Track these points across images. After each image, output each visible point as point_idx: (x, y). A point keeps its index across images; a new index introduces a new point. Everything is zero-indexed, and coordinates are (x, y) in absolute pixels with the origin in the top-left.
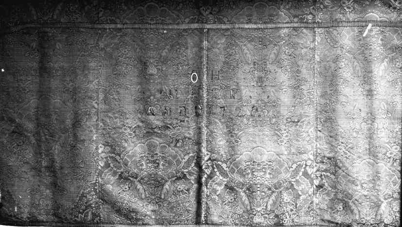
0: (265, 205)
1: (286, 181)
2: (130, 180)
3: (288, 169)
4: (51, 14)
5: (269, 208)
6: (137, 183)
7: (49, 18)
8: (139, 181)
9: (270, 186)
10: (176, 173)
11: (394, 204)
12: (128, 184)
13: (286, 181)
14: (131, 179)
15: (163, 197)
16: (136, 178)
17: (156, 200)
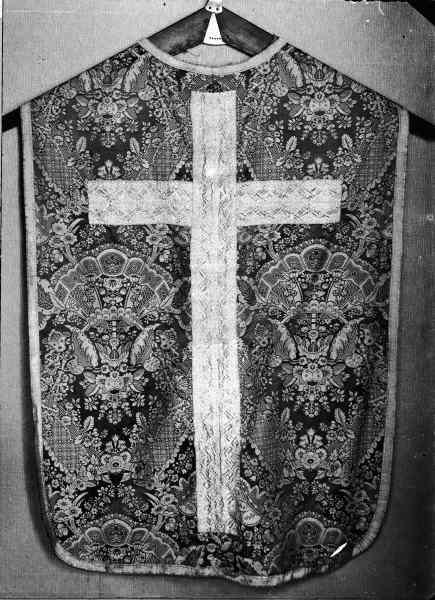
0: (326, 350)
1: (165, 313)
2: (68, 330)
3: (168, 288)
4: (120, 82)
5: (334, 356)
6: (83, 338)
7: (116, 89)
8: (87, 333)
9: (337, 315)
10: (364, 310)
11: (162, 337)
12: (64, 338)
13: (165, 313)
14: (72, 329)
15: (133, 362)
16: (81, 327)
17: (319, 362)
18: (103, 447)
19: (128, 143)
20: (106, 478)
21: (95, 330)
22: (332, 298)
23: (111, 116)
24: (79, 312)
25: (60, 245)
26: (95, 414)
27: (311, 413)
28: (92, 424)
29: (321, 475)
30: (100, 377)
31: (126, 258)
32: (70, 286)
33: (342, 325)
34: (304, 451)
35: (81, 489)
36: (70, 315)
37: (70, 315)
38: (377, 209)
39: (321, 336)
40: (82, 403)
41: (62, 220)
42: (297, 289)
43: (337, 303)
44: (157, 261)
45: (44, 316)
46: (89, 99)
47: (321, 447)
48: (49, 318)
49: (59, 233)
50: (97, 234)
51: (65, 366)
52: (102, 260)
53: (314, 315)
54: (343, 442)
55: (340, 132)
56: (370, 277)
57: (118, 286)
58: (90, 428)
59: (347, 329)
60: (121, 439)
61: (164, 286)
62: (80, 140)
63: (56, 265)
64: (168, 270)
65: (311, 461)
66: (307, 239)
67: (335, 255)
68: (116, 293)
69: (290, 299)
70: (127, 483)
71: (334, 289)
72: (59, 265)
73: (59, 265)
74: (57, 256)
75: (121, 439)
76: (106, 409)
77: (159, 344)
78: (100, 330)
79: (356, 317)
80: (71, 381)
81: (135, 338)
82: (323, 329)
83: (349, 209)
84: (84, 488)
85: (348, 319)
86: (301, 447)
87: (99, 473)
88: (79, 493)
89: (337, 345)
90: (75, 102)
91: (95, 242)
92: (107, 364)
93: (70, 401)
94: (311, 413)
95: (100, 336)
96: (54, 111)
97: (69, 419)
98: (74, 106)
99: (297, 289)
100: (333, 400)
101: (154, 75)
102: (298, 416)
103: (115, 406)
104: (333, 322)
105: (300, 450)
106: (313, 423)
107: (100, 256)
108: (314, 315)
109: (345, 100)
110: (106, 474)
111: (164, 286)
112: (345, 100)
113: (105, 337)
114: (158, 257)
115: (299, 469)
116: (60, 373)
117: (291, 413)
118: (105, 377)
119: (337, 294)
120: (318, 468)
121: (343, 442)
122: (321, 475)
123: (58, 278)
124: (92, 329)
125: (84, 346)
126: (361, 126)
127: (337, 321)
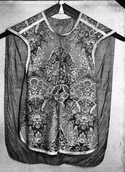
6: (77, 103)
12: (72, 103)
14: (74, 101)
18: (35, 135)
19: (37, 48)
20: (79, 144)
21: (81, 102)
22: (40, 93)
23: (92, 44)
24: (77, 96)
25: (74, 77)
26: (78, 125)
27: (38, 127)
28: (77, 128)
29: (84, 145)
30: (32, 115)
31: (38, 80)
32: (75, 89)
33: (44, 101)
34: (37, 138)
35: (71, 146)
36: (74, 97)
37: (74, 97)
38: (50, 67)
39: (88, 106)
40: (75, 122)
41: (75, 70)
42: (82, 92)
43: (42, 95)
44: (48, 81)
45: (67, 96)
46: (87, 38)
47: (85, 138)
48: (68, 96)
49: (74, 74)
50: (84, 75)
51: (71, 111)
52: (85, 82)
53: (36, 99)
54: (91, 137)
55: (37, 46)
56: (50, 87)
57: (36, 89)
58: (76, 129)
59: (45, 102)
60: (84, 134)
61: (50, 88)
62: (83, 50)
63: (72, 83)
64: (51, 83)
65: (82, 141)
66: (86, 77)
67: (40, 81)
68: (88, 92)
69: (80, 94)
70: (84, 147)
71: (40, 91)
72: (73, 83)
73: (73, 83)
74: (72, 80)
75: (84, 134)
76: (35, 124)
77: (50, 105)
78: (82, 102)
79: (47, 99)
80: (72, 115)
81: (43, 103)
82: (88, 105)
83: (43, 67)
84: (72, 146)
85: (45, 99)
86: (36, 137)
87: (34, 143)
88: (70, 147)
89: (43, 107)
90: (83, 39)
91: (83, 77)
92: (34, 111)
93: (71, 121)
94: (38, 127)
95: (82, 104)
96: (77, 40)
97: (70, 125)
98: (82, 40)
99: (82, 92)
100: (43, 123)
101: (22, 26)
102: (34, 129)
103: (38, 123)
104: (91, 103)
105: (35, 138)
106: (84, 131)
107: (31, 80)
108: (36, 99)
109: (38, 37)
110: (79, 142)
111: (50, 88)
112: (38, 37)
113: (83, 104)
114: (48, 80)
115: (36, 143)
116: (70, 112)
117: (32, 127)
118: (34, 115)
119: (41, 92)
120: (84, 143)
121: (91, 137)
122: (84, 145)
123: (72, 86)
124: (80, 101)
125: (77, 106)
126: (43, 44)
127: (93, 103)
